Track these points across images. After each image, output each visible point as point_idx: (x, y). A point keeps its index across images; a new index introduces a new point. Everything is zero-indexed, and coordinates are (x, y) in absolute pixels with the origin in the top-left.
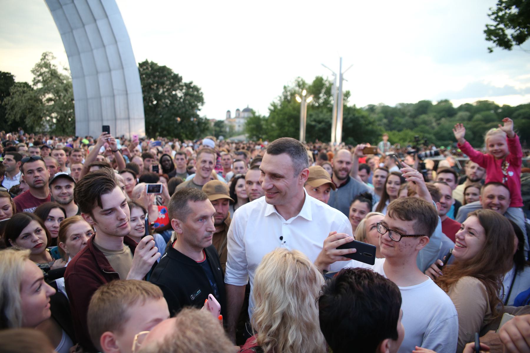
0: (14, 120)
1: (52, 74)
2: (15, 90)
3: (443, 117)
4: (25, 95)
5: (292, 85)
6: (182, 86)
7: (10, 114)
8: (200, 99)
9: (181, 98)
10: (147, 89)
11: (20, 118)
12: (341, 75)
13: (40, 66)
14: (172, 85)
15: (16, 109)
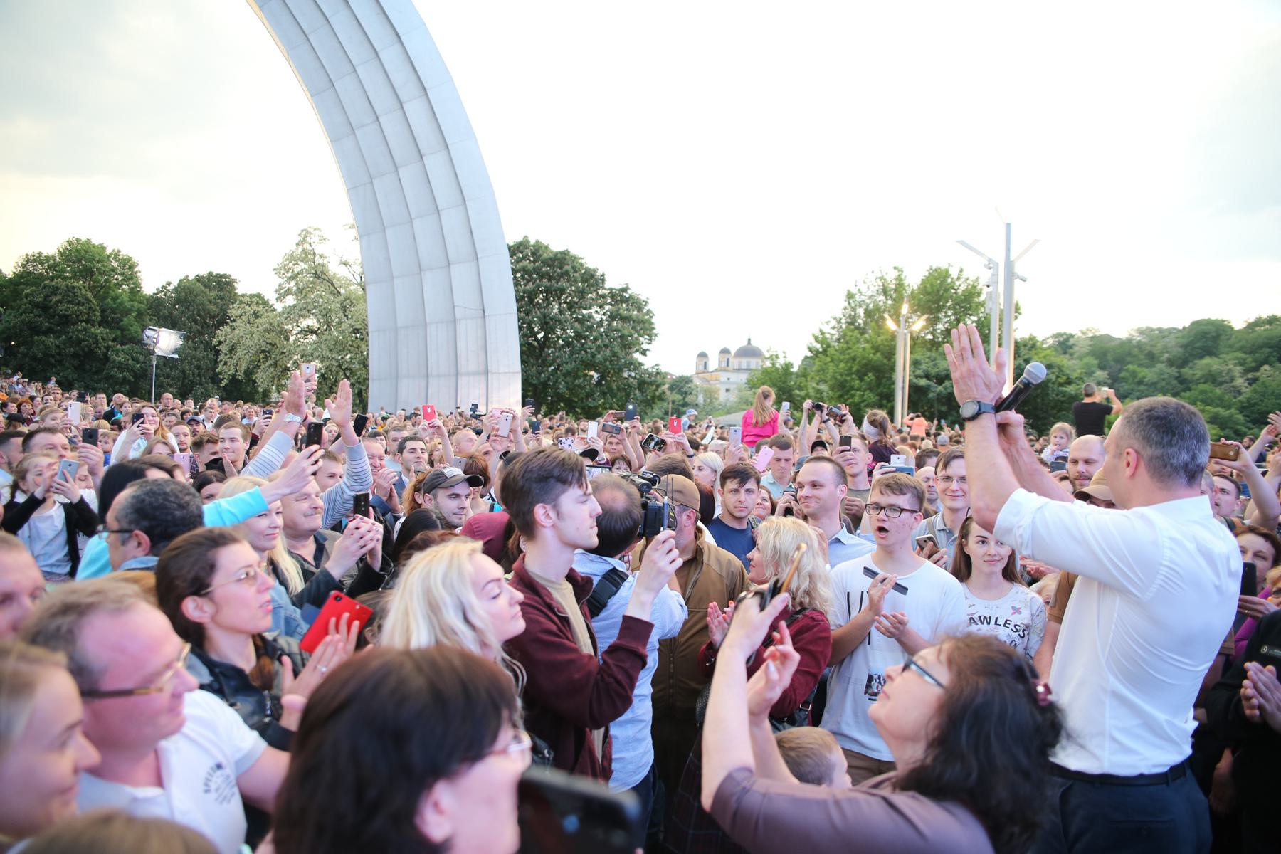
0: (234, 376)
1: (316, 276)
2: (239, 312)
3: (1266, 362)
4: (259, 321)
5: (869, 290)
6: (603, 296)
7: (226, 363)
8: (645, 327)
9: (600, 324)
10: (525, 302)
11: (245, 373)
12: (1009, 265)
13: (292, 258)
14: (582, 294)
15: (240, 353)
